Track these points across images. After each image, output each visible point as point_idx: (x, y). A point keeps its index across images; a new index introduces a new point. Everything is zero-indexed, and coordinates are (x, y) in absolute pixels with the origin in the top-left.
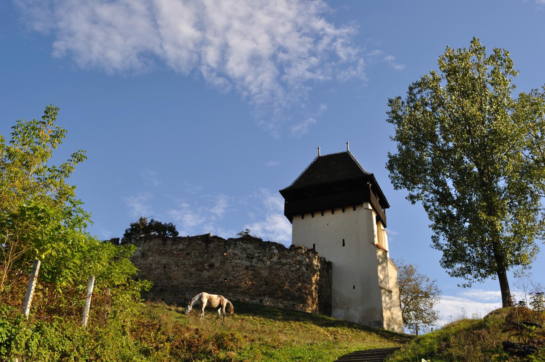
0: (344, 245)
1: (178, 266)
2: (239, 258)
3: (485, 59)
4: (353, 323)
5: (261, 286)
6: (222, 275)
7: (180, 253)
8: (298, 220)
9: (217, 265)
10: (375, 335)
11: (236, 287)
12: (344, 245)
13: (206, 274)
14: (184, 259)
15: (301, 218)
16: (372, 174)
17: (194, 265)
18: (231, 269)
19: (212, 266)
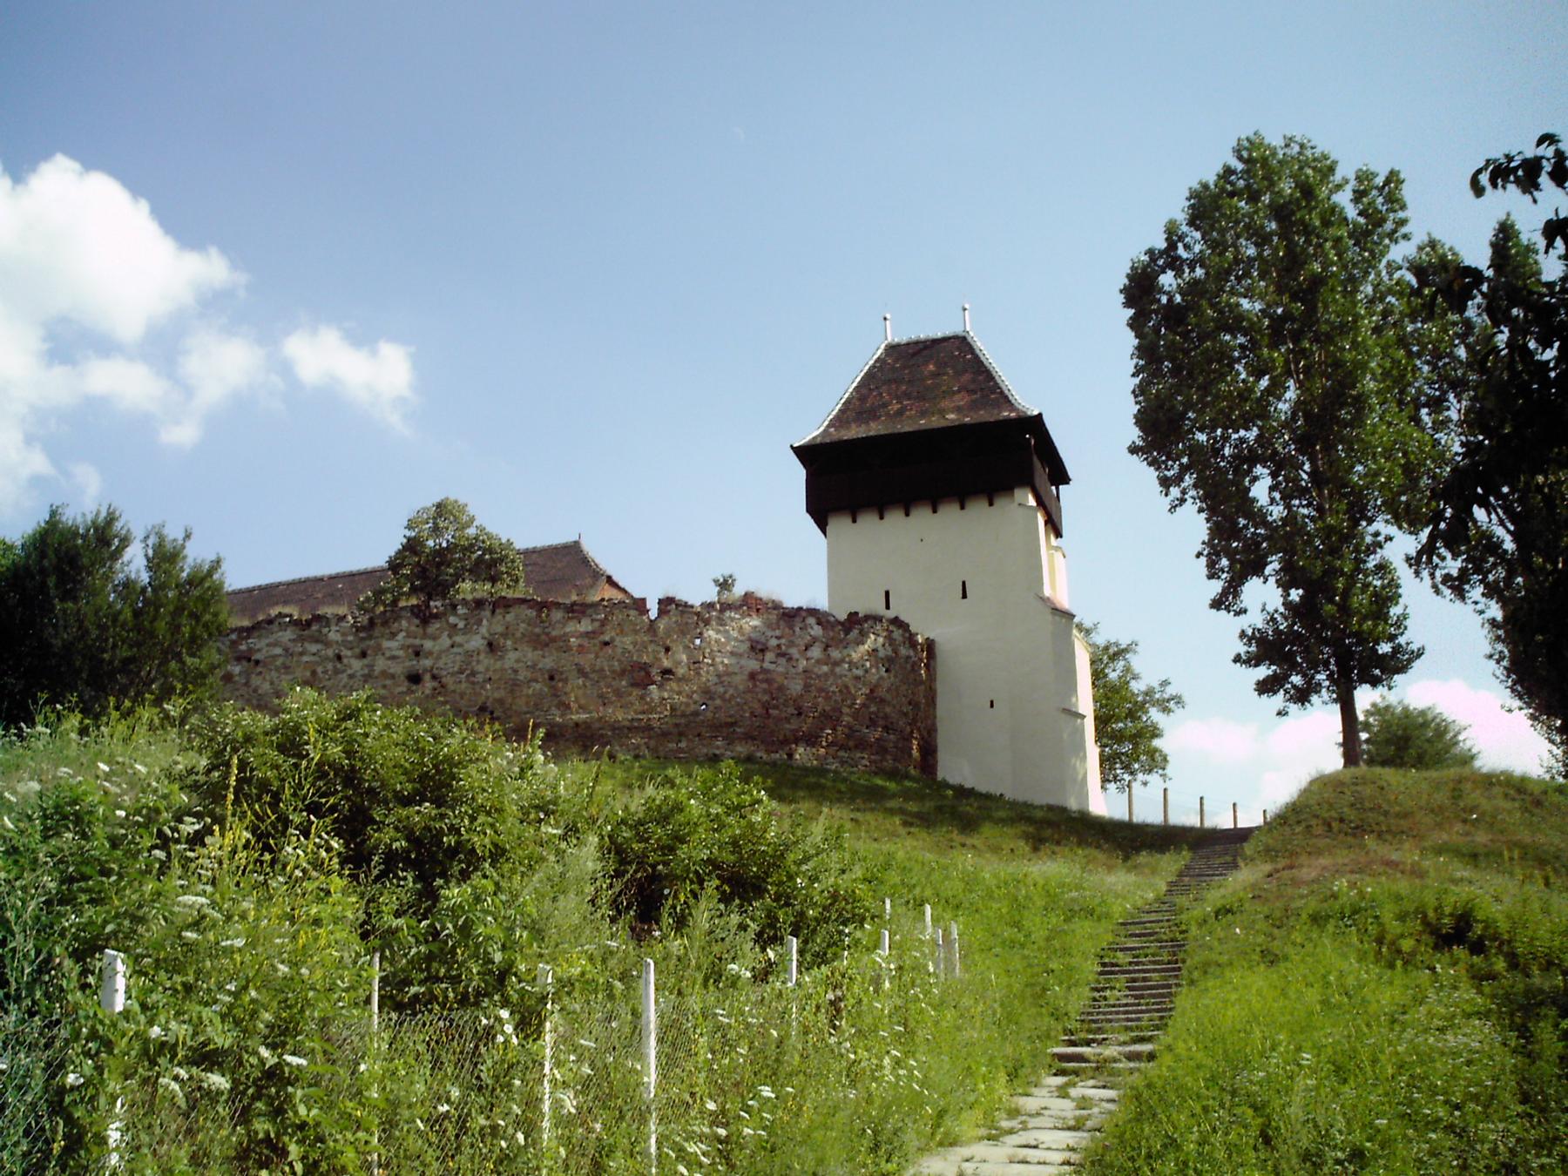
0: (964, 596)
7: (585, 642)
12: (964, 596)
14: (597, 657)
15: (876, 518)
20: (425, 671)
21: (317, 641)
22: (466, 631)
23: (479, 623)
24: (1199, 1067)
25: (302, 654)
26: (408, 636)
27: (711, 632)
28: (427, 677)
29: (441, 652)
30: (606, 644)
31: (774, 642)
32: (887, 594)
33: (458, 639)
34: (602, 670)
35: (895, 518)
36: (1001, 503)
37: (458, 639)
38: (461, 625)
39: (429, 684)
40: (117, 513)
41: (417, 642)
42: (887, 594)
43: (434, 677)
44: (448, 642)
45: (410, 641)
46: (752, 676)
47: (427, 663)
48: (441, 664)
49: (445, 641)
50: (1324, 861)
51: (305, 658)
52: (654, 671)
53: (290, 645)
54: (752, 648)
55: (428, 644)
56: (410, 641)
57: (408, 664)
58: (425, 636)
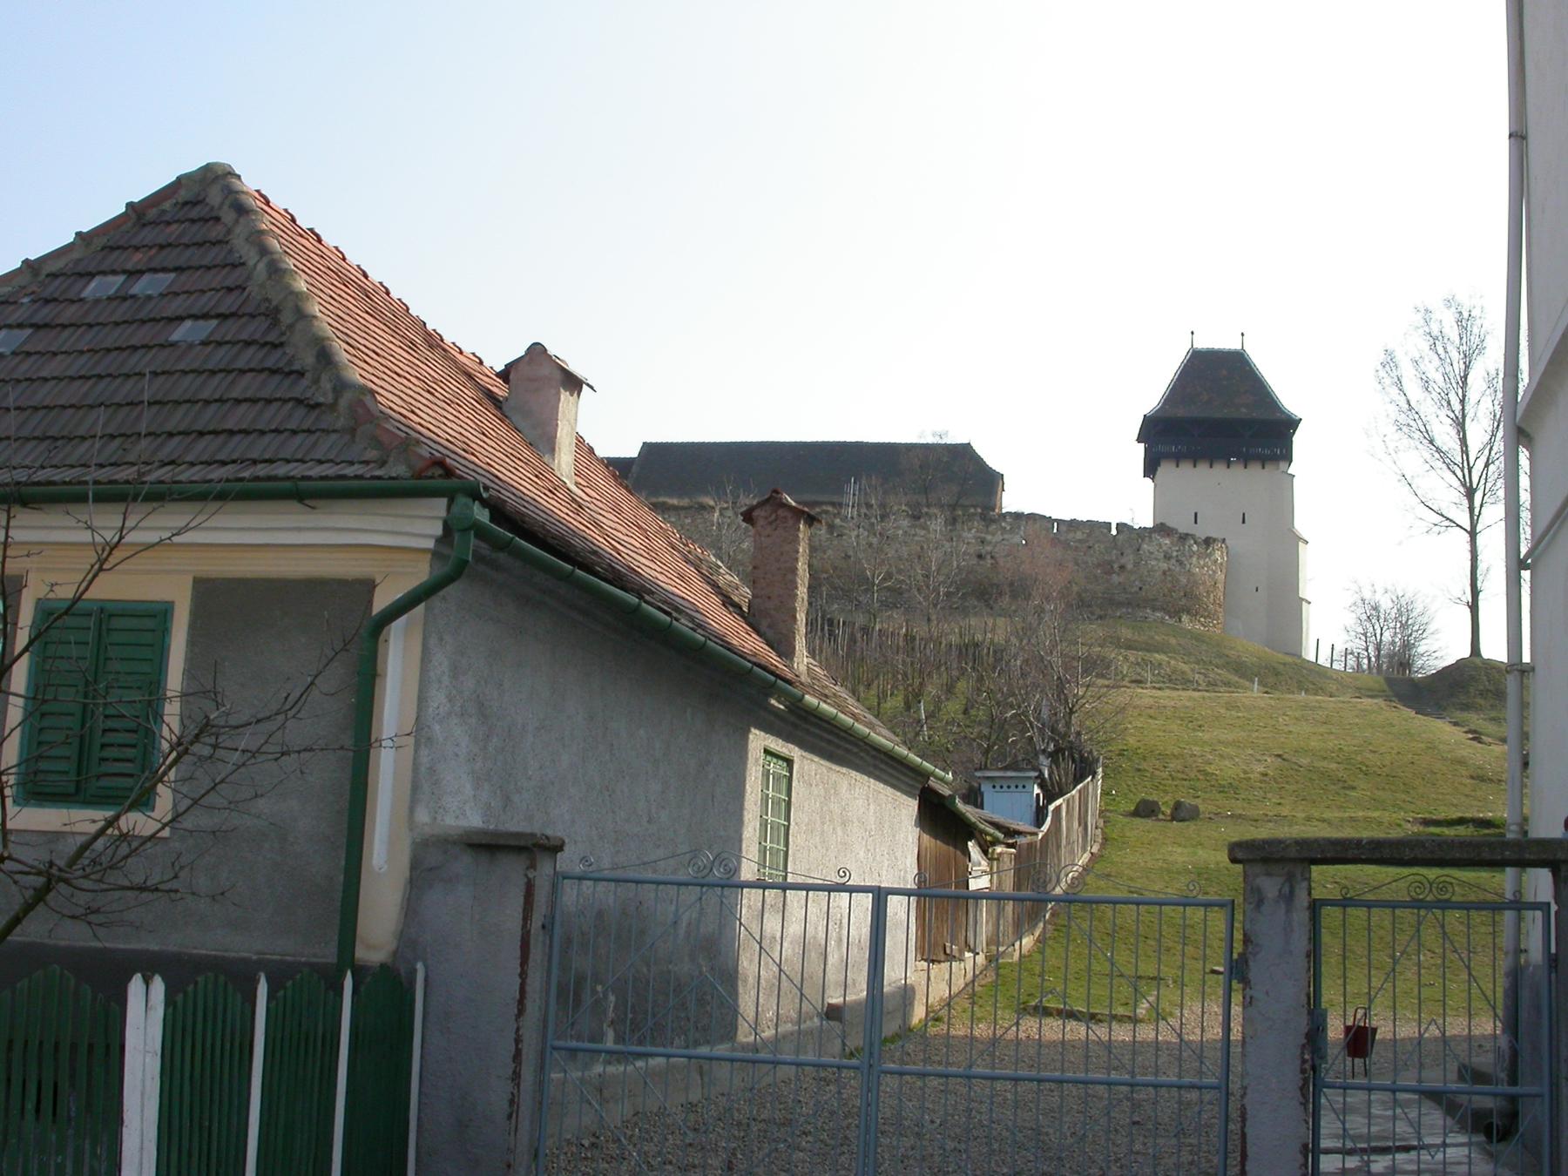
0: (1244, 522)
1: (1077, 564)
2: (1156, 559)
3: (1353, 756)
4: (514, 1072)
5: (1180, 600)
6: (1137, 583)
7: (1079, 545)
8: (1180, 475)
9: (1130, 566)
10: (1028, 1017)
11: (1153, 600)
12: (1244, 522)
13: (1116, 579)
14: (1085, 555)
15: (1174, 465)
16: (1291, 424)
17: (1099, 565)
18: (1146, 573)
19: (1122, 567)
20: (987, 553)
21: (924, 529)
22: (1012, 531)
23: (1019, 528)
24: (966, 737)
25: (914, 535)
26: (977, 532)
27: (1145, 546)
28: (989, 557)
29: (997, 542)
30: (1090, 547)
31: (1175, 554)
32: (1196, 514)
33: (1006, 536)
34: (1087, 563)
35: (1203, 468)
36: (1269, 467)
37: (1006, 536)
38: (1008, 528)
39: (989, 561)
40: (1431, 628)
41: (983, 535)
42: (1196, 514)
43: (992, 557)
44: (1001, 538)
45: (979, 534)
46: (1164, 573)
47: (989, 548)
48: (996, 550)
49: (998, 537)
50: (1124, 610)
51: (916, 538)
52: (1116, 566)
53: (908, 530)
54: (1165, 556)
55: (989, 537)
56: (979, 534)
57: (977, 548)
58: (987, 533)
